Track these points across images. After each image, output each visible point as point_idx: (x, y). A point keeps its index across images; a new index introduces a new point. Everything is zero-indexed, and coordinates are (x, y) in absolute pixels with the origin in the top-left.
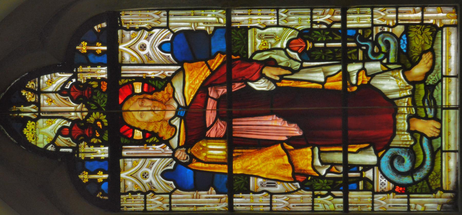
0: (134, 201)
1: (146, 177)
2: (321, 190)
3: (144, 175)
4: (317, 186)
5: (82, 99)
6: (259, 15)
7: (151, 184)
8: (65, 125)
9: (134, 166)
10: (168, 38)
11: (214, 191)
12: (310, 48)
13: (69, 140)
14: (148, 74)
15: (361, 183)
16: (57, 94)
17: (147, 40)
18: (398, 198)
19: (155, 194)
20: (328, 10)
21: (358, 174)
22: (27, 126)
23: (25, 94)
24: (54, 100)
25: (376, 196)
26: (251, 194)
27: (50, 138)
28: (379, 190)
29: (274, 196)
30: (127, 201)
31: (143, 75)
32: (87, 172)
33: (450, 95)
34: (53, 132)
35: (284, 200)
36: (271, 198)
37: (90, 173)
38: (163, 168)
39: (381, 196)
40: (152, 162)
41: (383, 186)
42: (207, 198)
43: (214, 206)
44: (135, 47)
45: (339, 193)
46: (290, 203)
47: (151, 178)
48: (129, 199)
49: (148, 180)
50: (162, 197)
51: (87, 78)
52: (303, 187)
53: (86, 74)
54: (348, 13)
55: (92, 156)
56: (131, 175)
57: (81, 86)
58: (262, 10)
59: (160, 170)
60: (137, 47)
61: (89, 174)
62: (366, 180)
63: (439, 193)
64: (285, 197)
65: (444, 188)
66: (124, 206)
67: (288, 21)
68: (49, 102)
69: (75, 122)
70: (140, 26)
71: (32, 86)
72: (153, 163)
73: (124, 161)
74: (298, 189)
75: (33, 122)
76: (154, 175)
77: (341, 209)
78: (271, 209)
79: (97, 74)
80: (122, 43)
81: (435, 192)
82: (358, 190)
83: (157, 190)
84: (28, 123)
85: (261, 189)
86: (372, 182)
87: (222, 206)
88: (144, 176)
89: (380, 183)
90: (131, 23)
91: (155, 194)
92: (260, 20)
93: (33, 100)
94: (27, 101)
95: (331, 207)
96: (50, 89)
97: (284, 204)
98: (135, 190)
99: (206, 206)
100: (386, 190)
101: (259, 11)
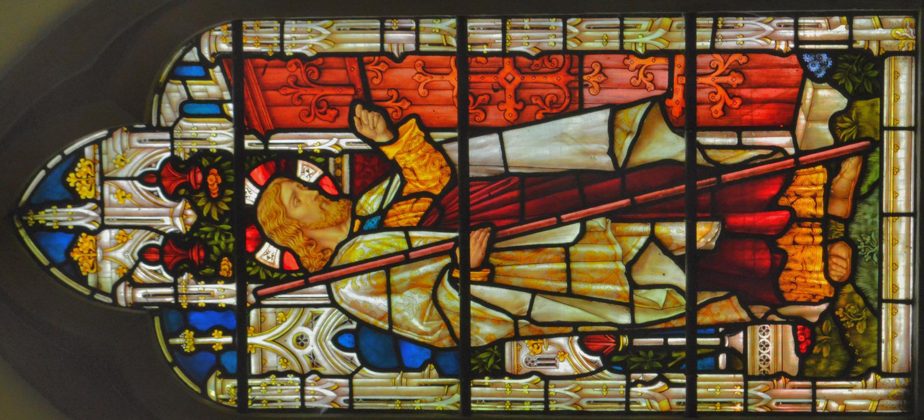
0: (281, 390)
1: (302, 345)
2: (641, 370)
3: (299, 341)
4: (634, 363)
5: (185, 265)
6: (527, 29)
7: (314, 318)
8: (153, 242)
9: (280, 322)
10: (352, 358)
11: (434, 372)
12: (624, 346)
13: (155, 193)
14: (307, 146)
15: (722, 359)
16: (136, 182)
17: (309, 328)
18: (794, 388)
19: (322, 376)
20: (658, 21)
21: (715, 341)
22: (79, 245)
23: (75, 183)
24: (130, 193)
25: (751, 383)
26: (507, 380)
27: (123, 268)
28: (757, 373)
29: (551, 382)
30: (267, 390)
31: (297, 147)
32: (193, 331)
33: (899, 102)
34: (130, 257)
35: (570, 390)
36: (546, 387)
37: (199, 334)
38: (336, 328)
39: (761, 385)
40: (313, 314)
41: (764, 349)
42: (421, 385)
43: (434, 401)
44: (285, 341)
45: (680, 378)
46: (583, 397)
47: (312, 347)
48: (271, 385)
49: (308, 350)
50: (336, 383)
51: (190, 149)
52: (608, 365)
53: (188, 143)
54: (699, 27)
55: (202, 302)
56: (274, 341)
57: (182, 166)
58: (532, 20)
59: (329, 334)
60: (290, 341)
61: (196, 336)
62: (732, 353)
63: (872, 379)
64: (572, 384)
65: (884, 369)
66: (262, 400)
67: (581, 42)
68: (120, 197)
69: (173, 238)
70: (294, 50)
71: (89, 168)
72: (316, 317)
73: (261, 313)
74: (599, 370)
75: (90, 237)
76: (319, 340)
77: (682, 408)
78: (547, 408)
79: (210, 142)
80: (261, 332)
81: (864, 376)
82: (715, 370)
83: (325, 369)
84: (80, 162)
85: (526, 369)
86: (743, 356)
87: (451, 402)
88: (300, 343)
89: (758, 357)
90: (279, 385)
91: (322, 376)
92: (529, 39)
93: (91, 195)
94: (81, 274)
95: (663, 405)
96: (123, 173)
97: (571, 397)
98: (281, 368)
99: (419, 401)
100: (771, 372)
101: (526, 23)
